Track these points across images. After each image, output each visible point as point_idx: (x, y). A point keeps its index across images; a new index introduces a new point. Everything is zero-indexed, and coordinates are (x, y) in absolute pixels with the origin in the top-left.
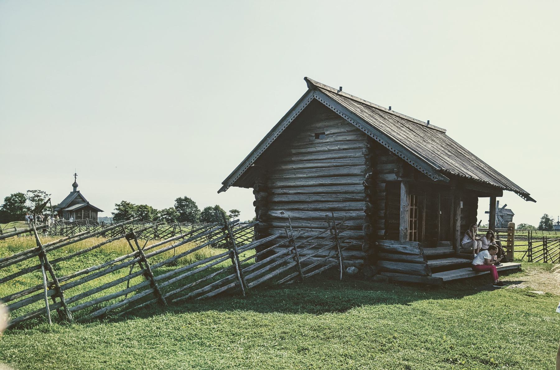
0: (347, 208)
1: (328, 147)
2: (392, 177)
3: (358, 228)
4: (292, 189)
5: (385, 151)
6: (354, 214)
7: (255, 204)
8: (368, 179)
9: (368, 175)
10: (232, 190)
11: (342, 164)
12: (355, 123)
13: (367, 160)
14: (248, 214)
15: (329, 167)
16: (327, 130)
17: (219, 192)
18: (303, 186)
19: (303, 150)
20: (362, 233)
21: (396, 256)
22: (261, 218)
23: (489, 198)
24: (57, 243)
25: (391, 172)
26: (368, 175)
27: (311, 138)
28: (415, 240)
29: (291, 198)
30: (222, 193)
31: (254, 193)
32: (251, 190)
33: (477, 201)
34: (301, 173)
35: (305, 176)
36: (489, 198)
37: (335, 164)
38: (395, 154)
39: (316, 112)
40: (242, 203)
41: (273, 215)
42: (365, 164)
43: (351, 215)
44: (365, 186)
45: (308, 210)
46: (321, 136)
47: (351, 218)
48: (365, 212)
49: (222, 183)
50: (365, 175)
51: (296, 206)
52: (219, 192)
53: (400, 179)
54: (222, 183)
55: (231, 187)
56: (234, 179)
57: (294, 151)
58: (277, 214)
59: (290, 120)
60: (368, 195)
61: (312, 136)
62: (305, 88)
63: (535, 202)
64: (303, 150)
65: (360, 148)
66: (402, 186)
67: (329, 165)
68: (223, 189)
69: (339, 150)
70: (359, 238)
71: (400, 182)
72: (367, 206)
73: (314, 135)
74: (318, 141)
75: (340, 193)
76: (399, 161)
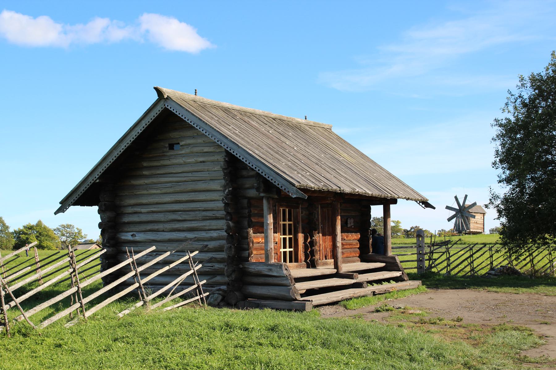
0: (207, 228)
1: (184, 159)
2: (252, 193)
3: (219, 249)
4: (144, 207)
5: (245, 167)
6: (214, 234)
7: (100, 226)
8: (227, 195)
9: (227, 190)
10: (74, 210)
11: (198, 179)
12: (210, 136)
13: (225, 174)
14: (94, 233)
15: (185, 181)
16: (182, 141)
17: (56, 213)
18: (157, 204)
19: (155, 164)
20: (222, 255)
21: (262, 280)
22: (108, 242)
23: (382, 206)
24: (388, 280)
25: (252, 188)
26: (227, 190)
27: (165, 150)
28: (291, 261)
29: (144, 218)
30: (60, 214)
31: (100, 212)
32: (96, 208)
33: (370, 209)
34: (157, 189)
35: (159, 191)
36: (382, 206)
37: (192, 178)
38: (253, 169)
39: (163, 129)
40: (87, 221)
41: (123, 238)
42: (224, 178)
43: (212, 235)
44: (225, 204)
45: (163, 231)
46: (176, 147)
47: (212, 239)
48: (226, 231)
49: (60, 203)
50: (224, 191)
51: (149, 227)
52: (56, 213)
53: (262, 195)
54: (60, 203)
55: (72, 207)
56: (75, 197)
57: (145, 164)
58: (127, 236)
59: (139, 130)
60: (228, 213)
61: (166, 147)
62: (155, 97)
63: (434, 208)
64: (155, 164)
65: (218, 161)
66: (265, 202)
67: (185, 179)
68: (61, 210)
69: (197, 162)
70: (221, 261)
71: (263, 197)
72: (228, 226)
73: (167, 145)
74: (172, 153)
75: (199, 210)
76: (258, 176)
